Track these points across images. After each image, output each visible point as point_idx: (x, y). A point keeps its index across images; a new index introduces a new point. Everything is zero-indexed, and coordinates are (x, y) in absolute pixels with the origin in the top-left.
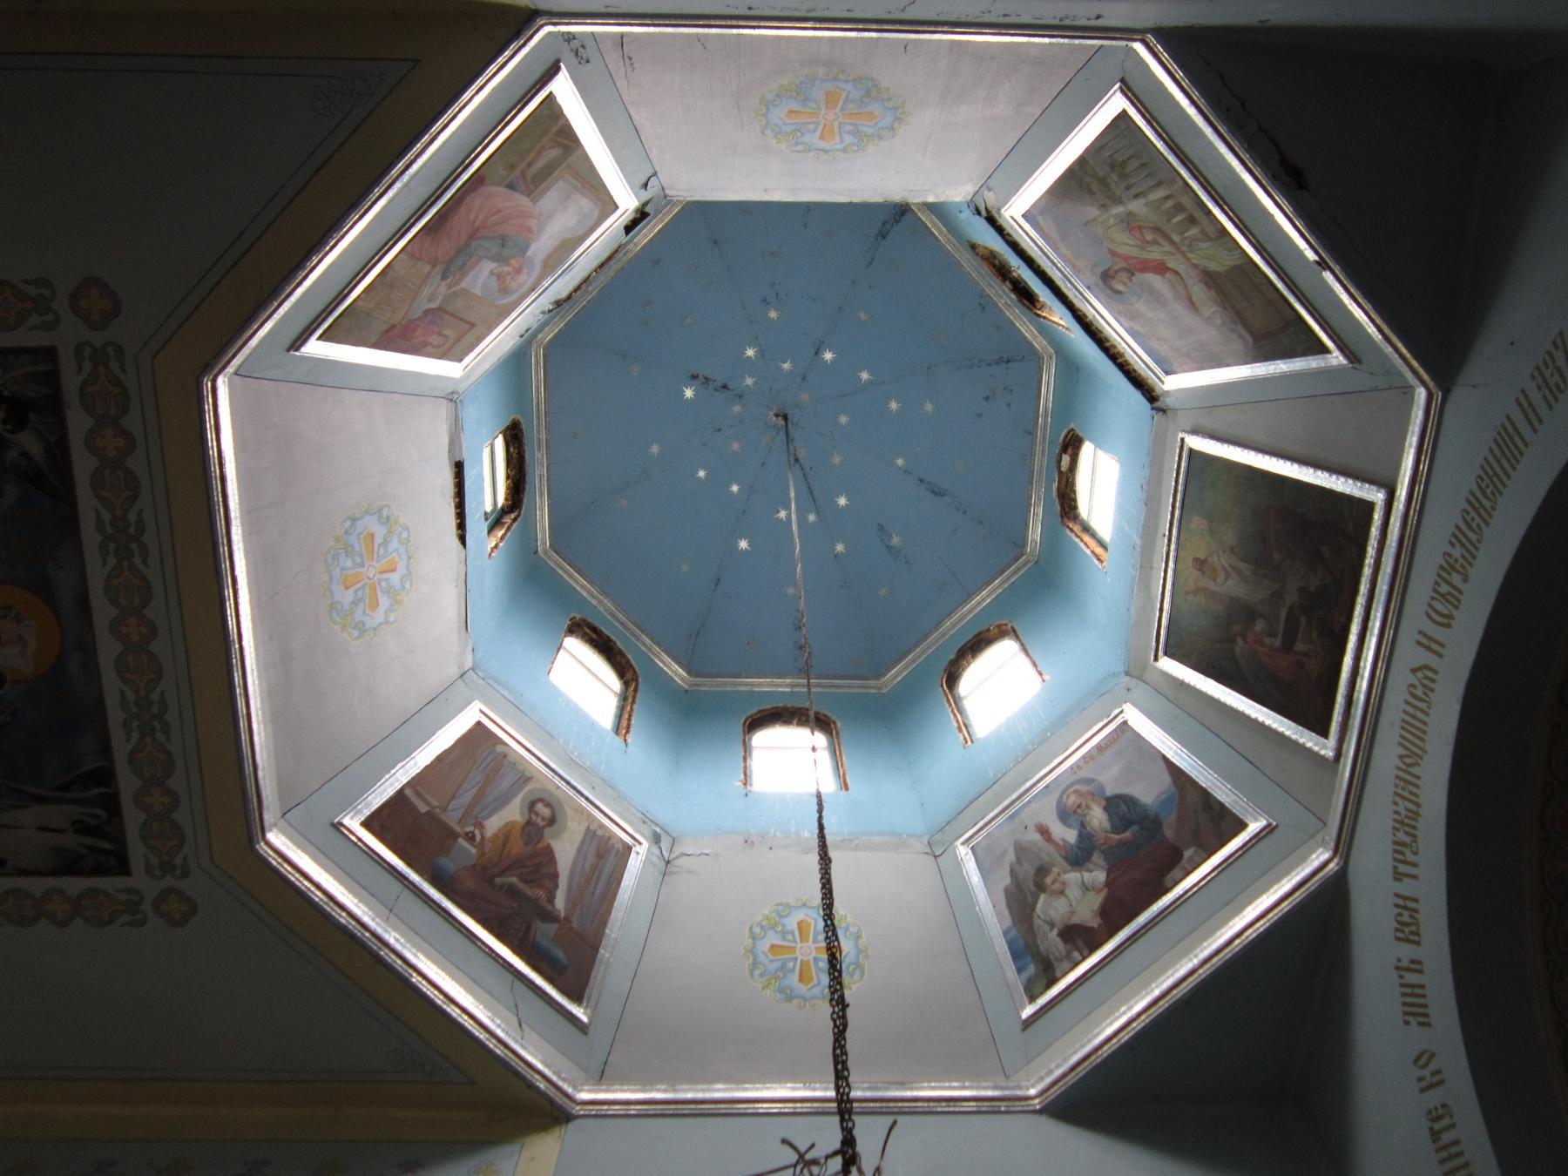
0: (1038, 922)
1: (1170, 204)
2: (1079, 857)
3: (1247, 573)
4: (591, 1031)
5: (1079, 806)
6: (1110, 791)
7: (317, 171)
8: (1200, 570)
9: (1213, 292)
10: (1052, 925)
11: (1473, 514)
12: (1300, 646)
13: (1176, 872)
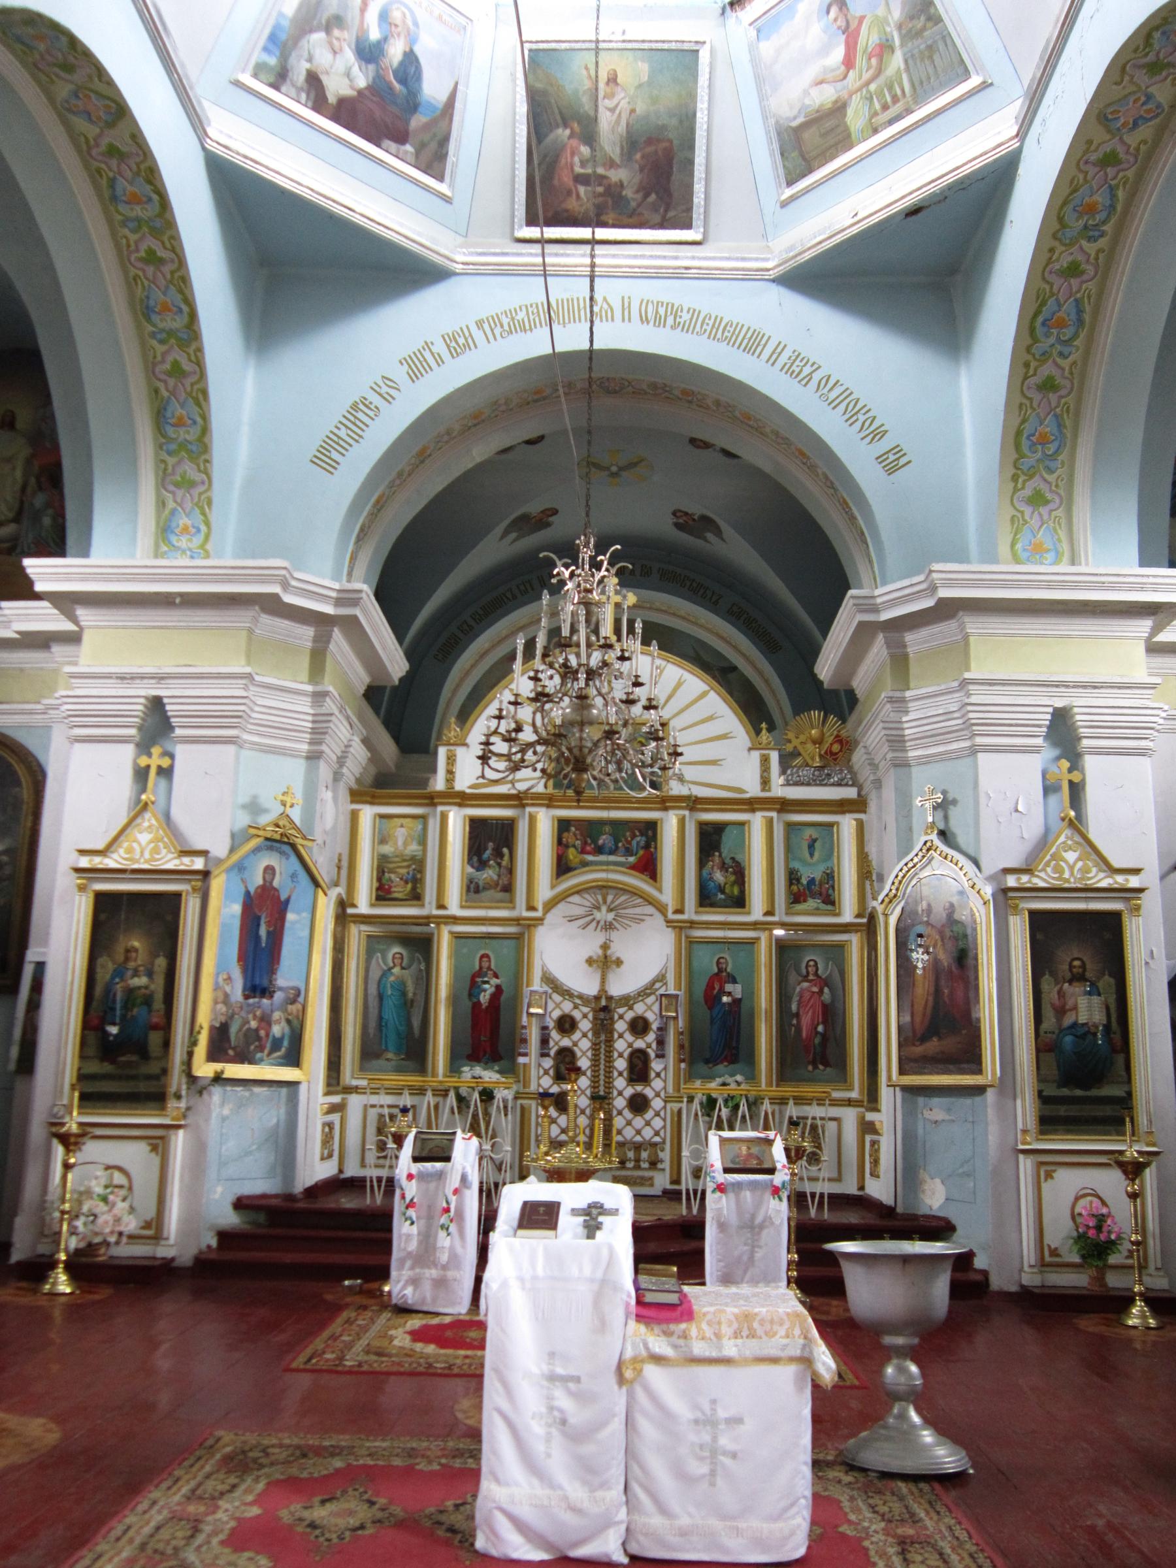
0: (304, 43)
1: (899, 92)
2: (369, 53)
3: (620, 129)
4: (455, 201)
5: (396, 26)
6: (417, 50)
7: (1095, 686)
8: (609, 80)
9: (830, 106)
10: (310, 59)
11: (711, 323)
12: (582, 189)
13: (393, 146)
